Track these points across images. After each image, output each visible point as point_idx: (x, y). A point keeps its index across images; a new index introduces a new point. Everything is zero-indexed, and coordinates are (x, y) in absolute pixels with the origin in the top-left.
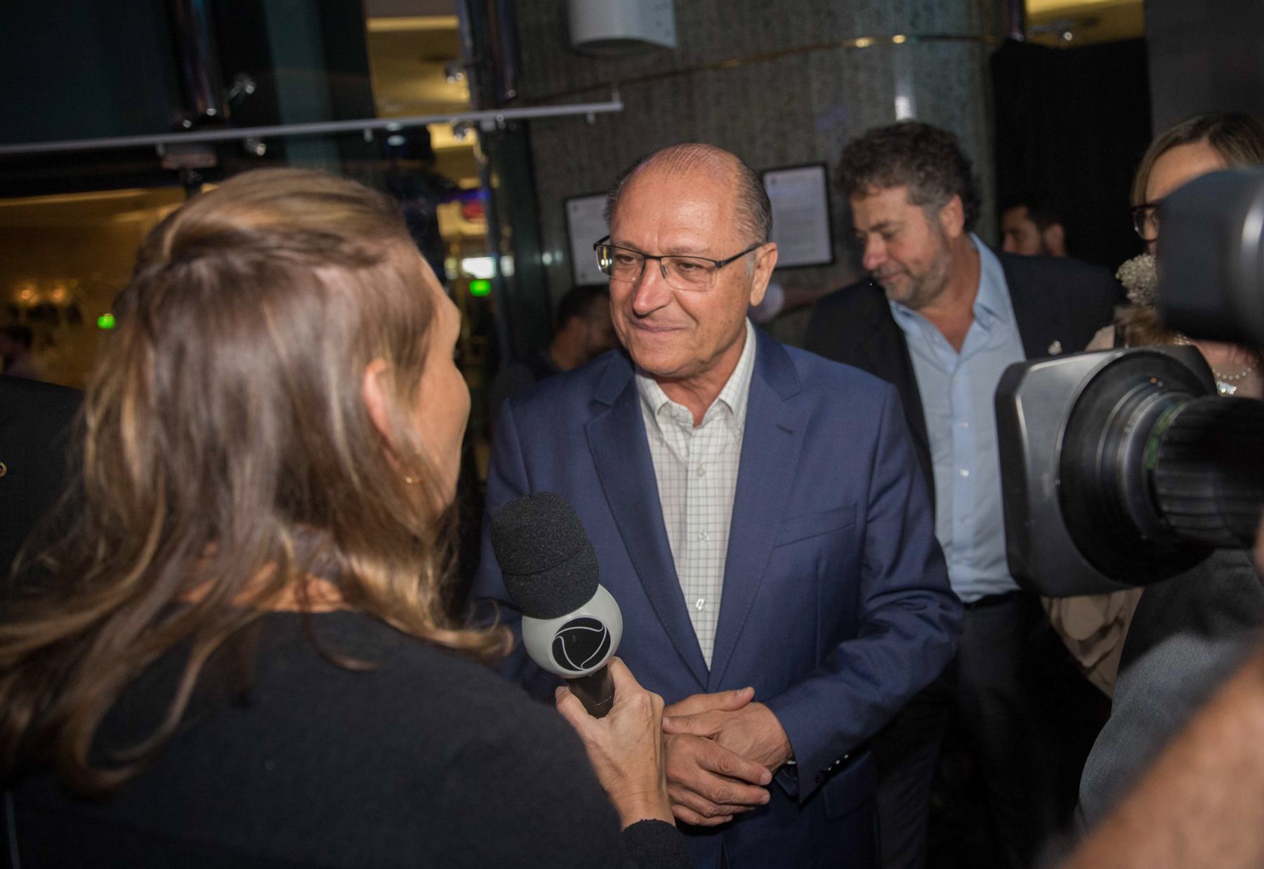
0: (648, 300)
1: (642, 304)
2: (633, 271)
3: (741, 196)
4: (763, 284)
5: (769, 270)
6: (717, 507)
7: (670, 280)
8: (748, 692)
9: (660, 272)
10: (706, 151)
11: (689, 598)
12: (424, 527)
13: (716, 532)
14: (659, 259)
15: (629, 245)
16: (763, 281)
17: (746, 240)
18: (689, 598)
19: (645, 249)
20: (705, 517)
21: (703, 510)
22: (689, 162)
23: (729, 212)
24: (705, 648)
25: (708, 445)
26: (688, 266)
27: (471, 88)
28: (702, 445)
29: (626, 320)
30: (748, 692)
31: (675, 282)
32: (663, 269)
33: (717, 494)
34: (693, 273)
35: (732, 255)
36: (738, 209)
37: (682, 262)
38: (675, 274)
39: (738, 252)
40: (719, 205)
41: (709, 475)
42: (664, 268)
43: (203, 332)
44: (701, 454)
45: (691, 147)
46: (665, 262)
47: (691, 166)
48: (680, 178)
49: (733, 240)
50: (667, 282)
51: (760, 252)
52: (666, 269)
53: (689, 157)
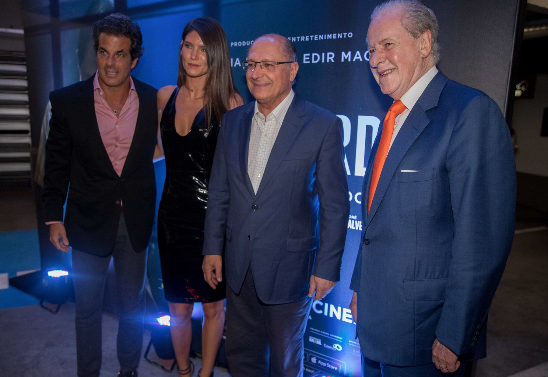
1: (254, 76)
3: (285, 46)
4: (294, 76)
5: (296, 71)
7: (263, 70)
9: (260, 67)
13: (262, 140)
14: (260, 63)
15: (251, 61)
16: (294, 74)
19: (256, 61)
21: (264, 147)
23: (281, 50)
24: (255, 188)
25: (270, 128)
26: (268, 65)
27: (163, 315)
28: (268, 128)
29: (251, 82)
31: (264, 70)
32: (261, 66)
34: (270, 67)
37: (267, 64)
38: (265, 68)
40: (278, 47)
41: (268, 137)
44: (267, 130)
45: (386, 4)
46: (262, 64)
51: (292, 64)
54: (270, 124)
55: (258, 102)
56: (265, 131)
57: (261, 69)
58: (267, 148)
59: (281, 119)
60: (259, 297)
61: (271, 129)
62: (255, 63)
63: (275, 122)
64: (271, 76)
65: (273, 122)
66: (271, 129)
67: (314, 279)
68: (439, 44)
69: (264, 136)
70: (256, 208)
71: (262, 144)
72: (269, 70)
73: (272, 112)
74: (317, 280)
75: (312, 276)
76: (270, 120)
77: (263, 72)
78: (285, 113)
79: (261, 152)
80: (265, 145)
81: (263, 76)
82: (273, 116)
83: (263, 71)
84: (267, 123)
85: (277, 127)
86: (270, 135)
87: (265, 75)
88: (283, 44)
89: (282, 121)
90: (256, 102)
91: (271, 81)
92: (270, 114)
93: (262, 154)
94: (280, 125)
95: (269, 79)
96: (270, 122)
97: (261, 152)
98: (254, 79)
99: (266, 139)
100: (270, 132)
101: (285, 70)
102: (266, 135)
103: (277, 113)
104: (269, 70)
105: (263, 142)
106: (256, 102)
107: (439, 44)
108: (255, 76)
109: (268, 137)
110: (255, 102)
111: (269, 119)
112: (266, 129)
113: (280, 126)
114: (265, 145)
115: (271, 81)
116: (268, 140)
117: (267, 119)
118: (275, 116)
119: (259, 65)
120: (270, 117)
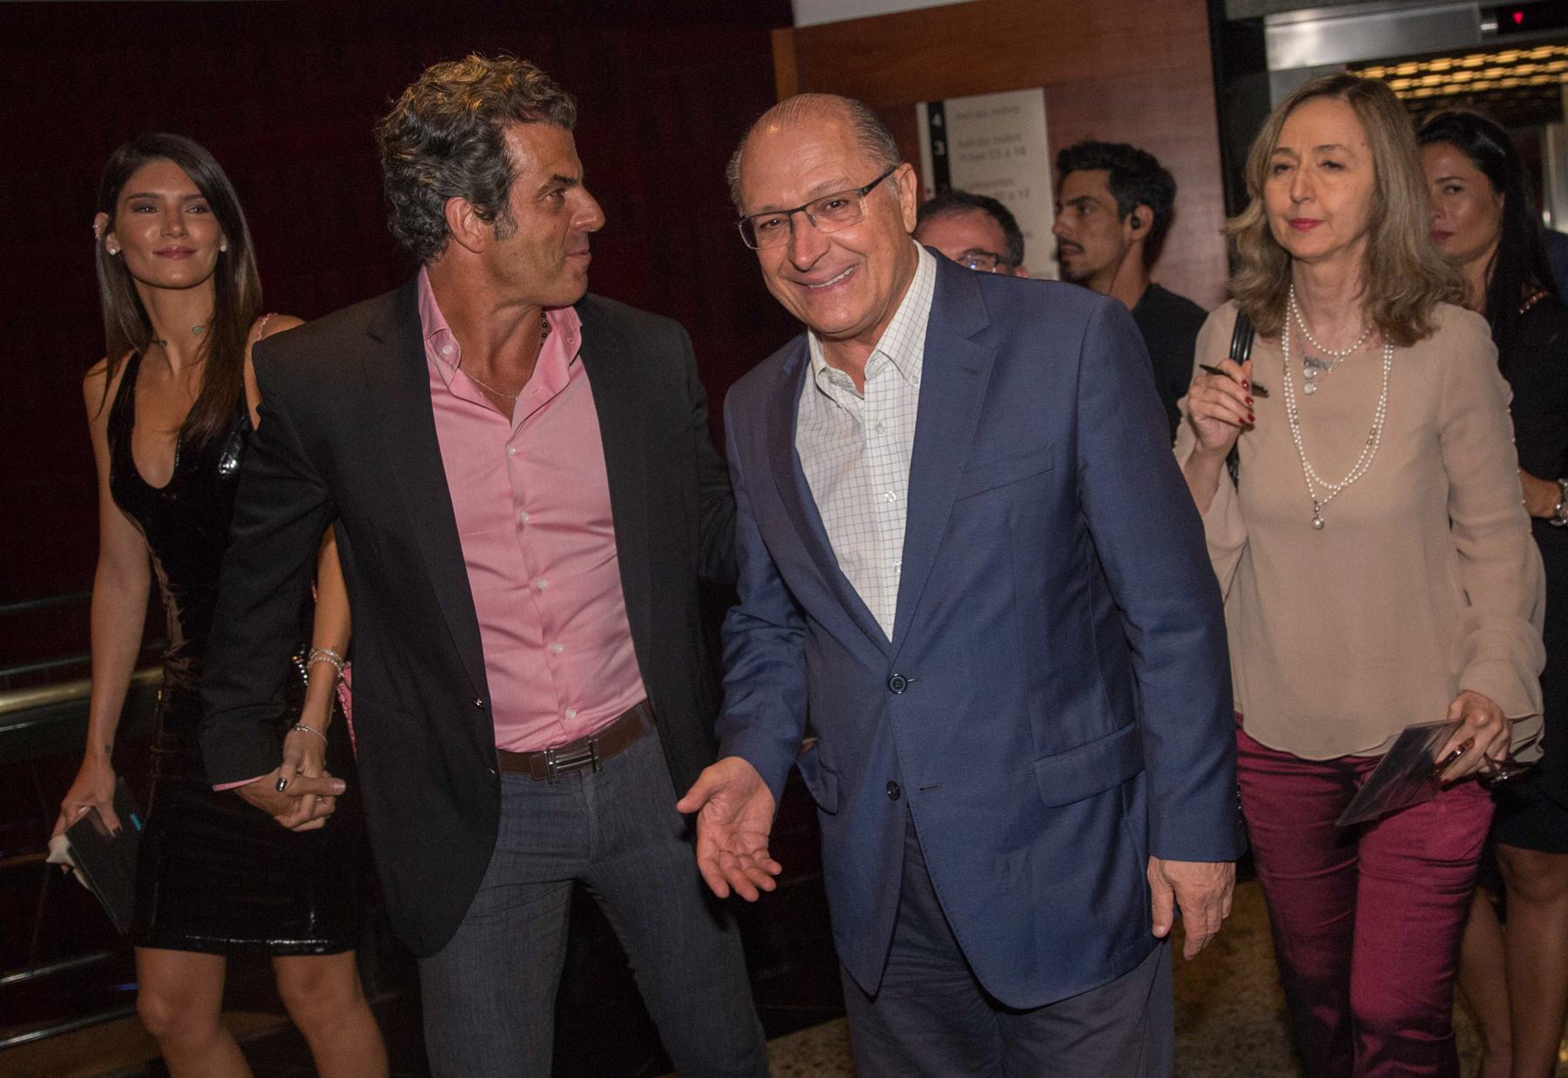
0: (810, 248)
2: (781, 234)
3: (859, 125)
4: (912, 209)
5: (912, 192)
6: (901, 463)
8: (1489, 794)
10: (808, 99)
11: (831, 533)
12: (1342, 94)
14: (803, 209)
15: (768, 211)
17: (879, 164)
18: (831, 533)
19: (789, 207)
20: (890, 475)
21: (887, 469)
22: (797, 111)
29: (786, 282)
30: (1489, 794)
31: (826, 227)
32: (810, 217)
33: (871, 460)
35: (870, 182)
36: (860, 137)
38: (825, 220)
39: (876, 178)
41: (890, 431)
42: (811, 217)
43: (1490, 797)
46: (809, 210)
47: (800, 114)
48: (795, 127)
49: (867, 167)
50: (819, 229)
51: (898, 174)
52: (814, 217)
53: (795, 106)
54: (881, 387)
55: (820, 335)
56: (872, 415)
57: (815, 229)
58: (895, 467)
59: (913, 359)
60: (990, 990)
61: (889, 404)
62: (784, 217)
63: (897, 374)
64: (850, 237)
65: (888, 376)
66: (889, 404)
67: (1162, 869)
68: (1243, 266)
69: (873, 433)
70: (903, 684)
71: (877, 461)
72: (841, 220)
73: (878, 346)
74: (1173, 875)
75: (1153, 861)
76: (877, 375)
77: (826, 235)
78: (923, 336)
79: (880, 489)
80: (885, 460)
81: (829, 247)
82: (886, 359)
83: (823, 233)
84: (868, 387)
85: (908, 390)
86: (890, 423)
87: (832, 243)
88: (852, 123)
89: (920, 364)
90: (811, 336)
91: (859, 253)
92: (874, 352)
93: (887, 495)
94: (917, 382)
95: (850, 250)
96: (880, 378)
97: (880, 489)
98: (804, 268)
99: (882, 441)
100: (889, 413)
101: (886, 204)
102: (880, 425)
103: (896, 345)
104: (841, 220)
105: (875, 452)
106: (811, 336)
107: (1243, 266)
108: (804, 259)
109: (890, 431)
110: (806, 335)
111: (873, 370)
112: (873, 406)
113: (918, 386)
114: (885, 460)
115: (859, 253)
116: (890, 439)
117: (868, 371)
118: (893, 355)
119: (805, 218)
120: (876, 364)
